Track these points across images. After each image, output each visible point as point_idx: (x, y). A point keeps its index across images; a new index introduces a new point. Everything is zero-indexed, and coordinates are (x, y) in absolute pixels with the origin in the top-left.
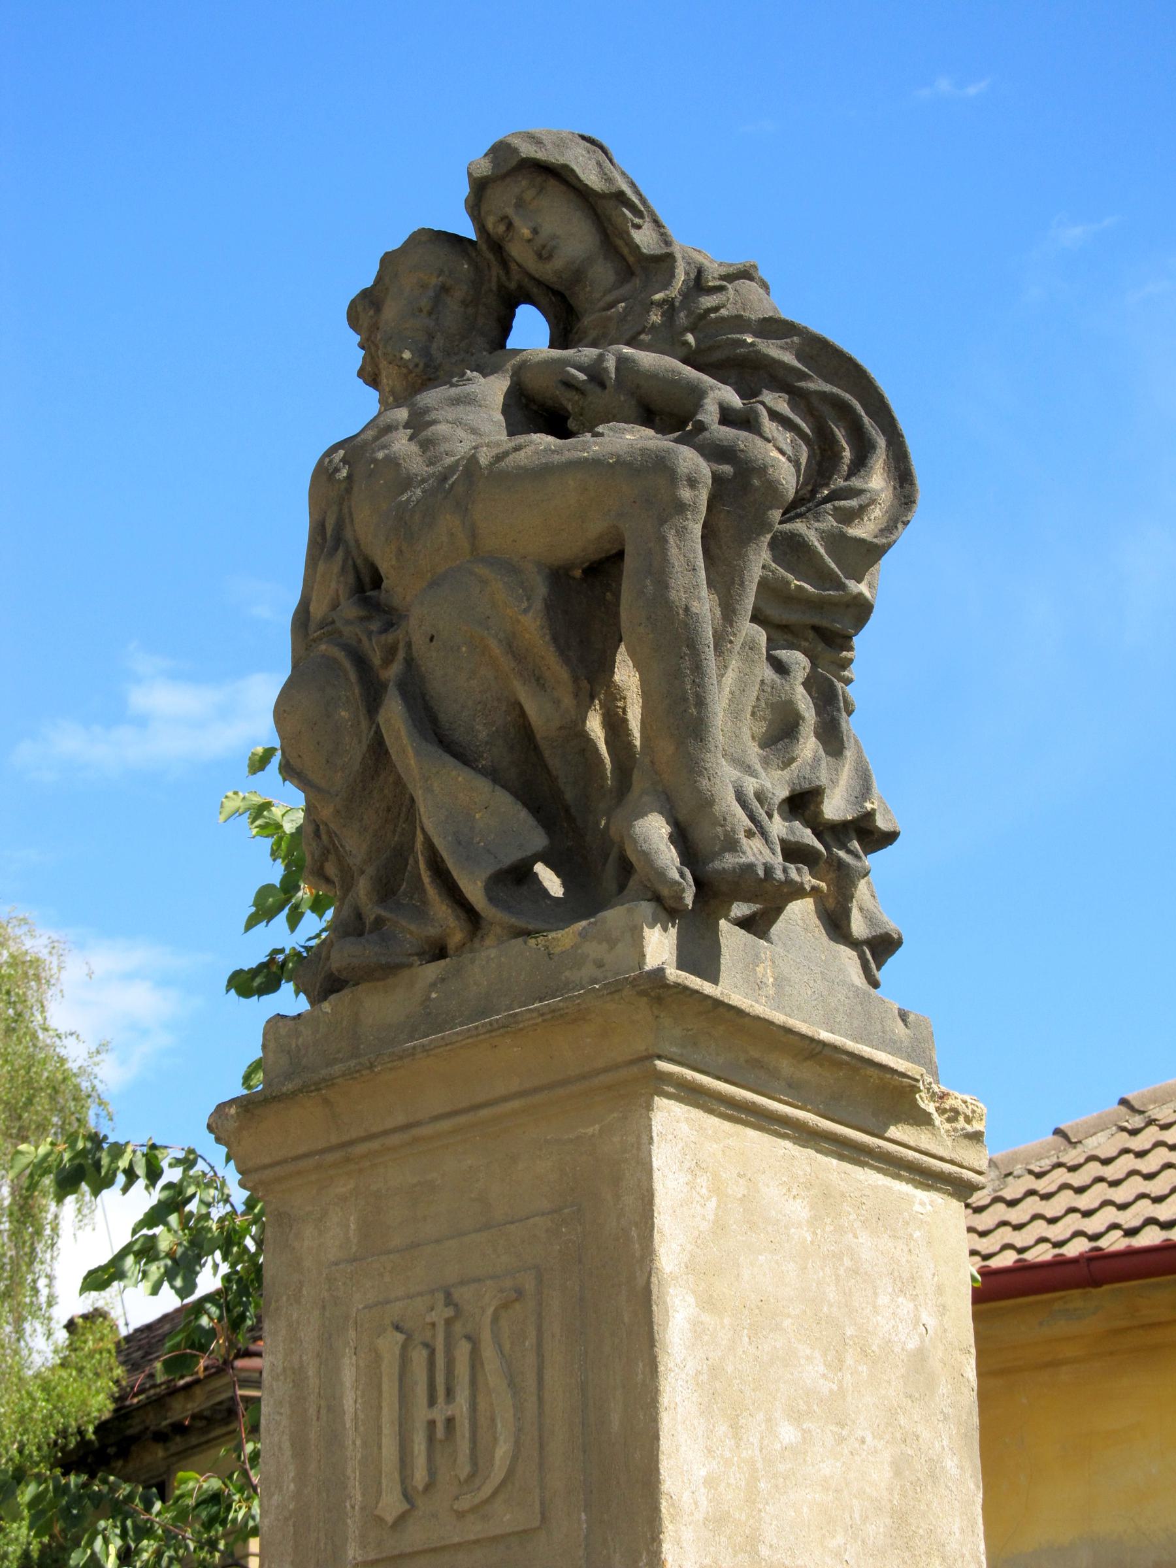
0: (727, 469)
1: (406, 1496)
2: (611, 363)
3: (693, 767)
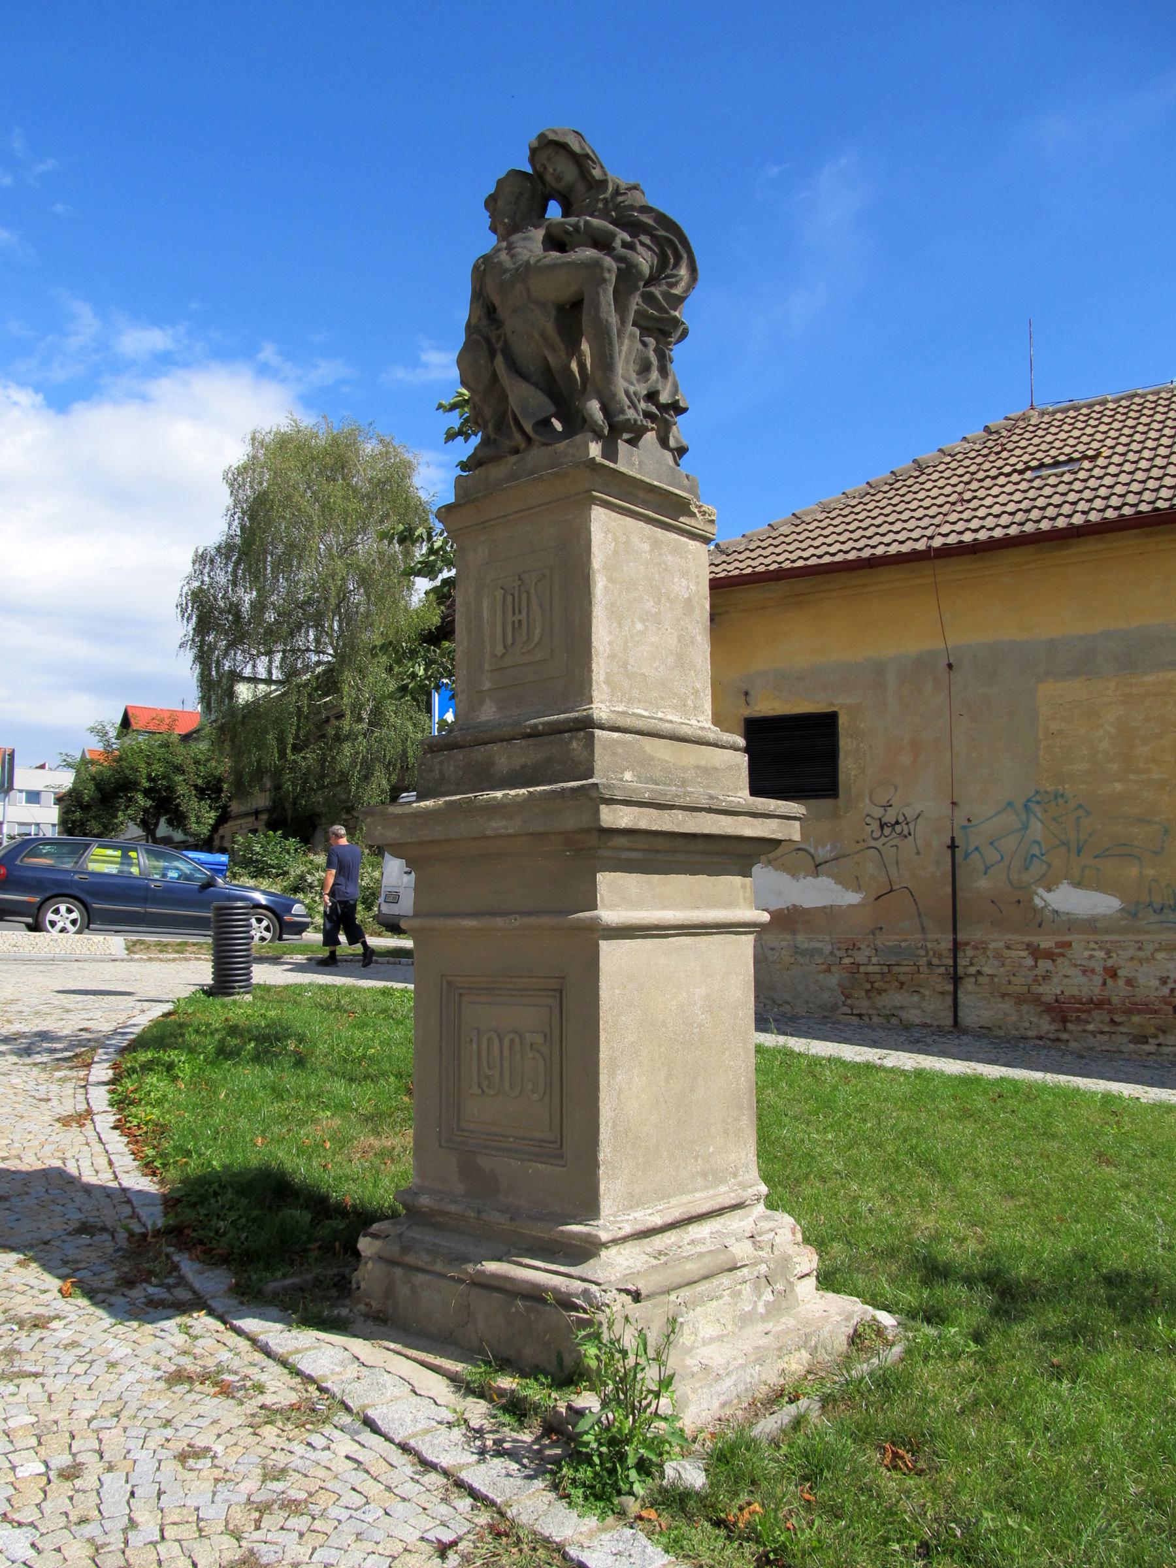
0: (623, 266)
1: (505, 647)
2: (582, 224)
3: (608, 380)
